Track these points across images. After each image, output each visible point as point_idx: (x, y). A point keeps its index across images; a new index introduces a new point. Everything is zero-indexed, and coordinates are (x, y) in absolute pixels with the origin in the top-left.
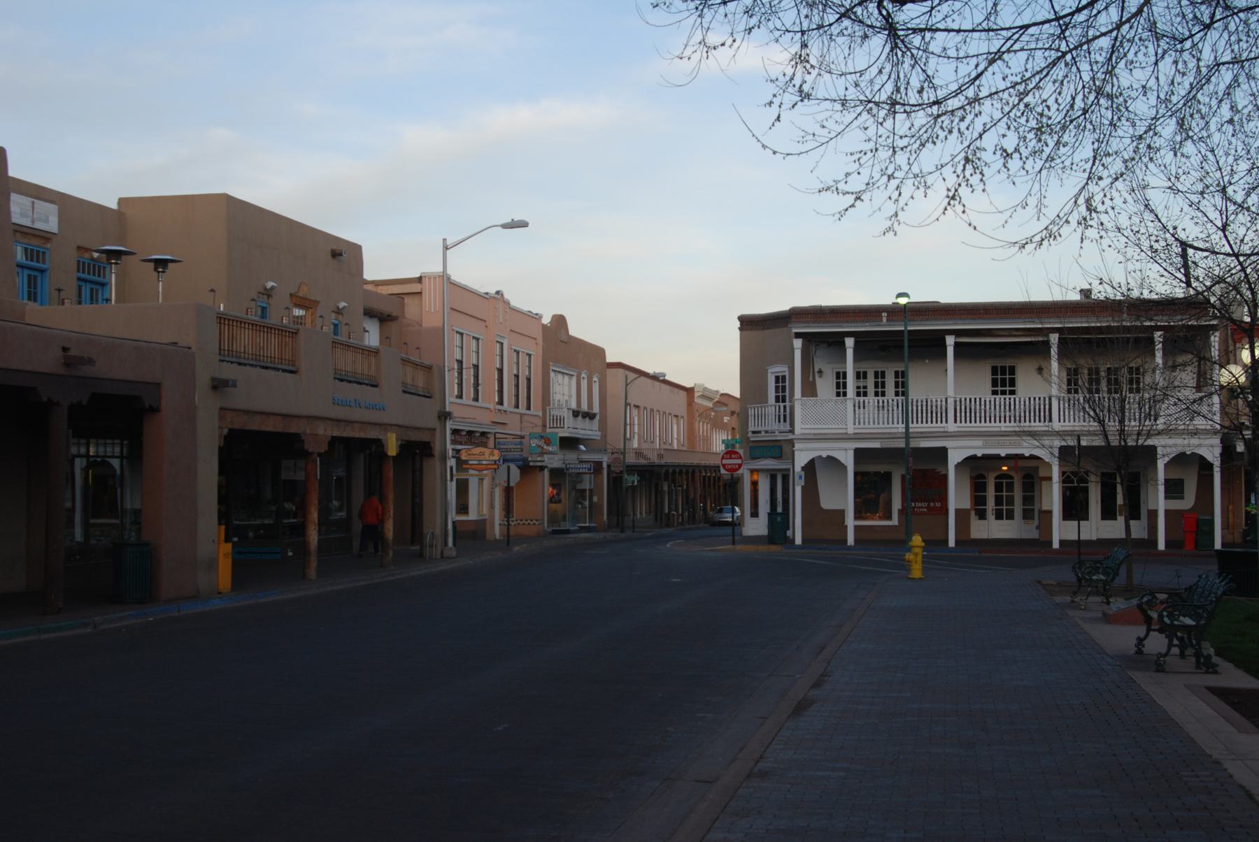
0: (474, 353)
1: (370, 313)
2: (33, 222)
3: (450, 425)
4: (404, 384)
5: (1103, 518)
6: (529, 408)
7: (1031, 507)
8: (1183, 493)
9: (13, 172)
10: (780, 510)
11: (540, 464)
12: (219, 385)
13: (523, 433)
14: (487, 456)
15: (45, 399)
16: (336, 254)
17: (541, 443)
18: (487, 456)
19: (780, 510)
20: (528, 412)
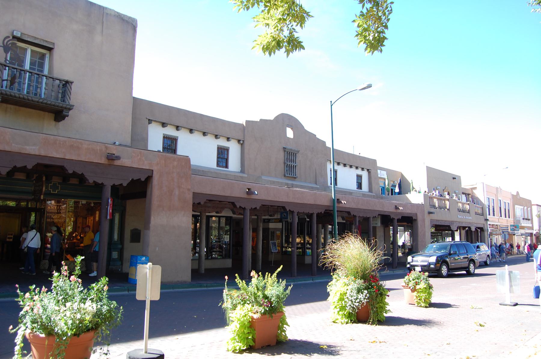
0: (38, 100)
1: (463, 193)
2: (381, 176)
3: (489, 223)
4: (476, 212)
5: (192, 215)
6: (509, 218)
7: (31, 66)
8: (135, 290)
9: (378, 165)
10: (116, 237)
11: (514, 234)
12: (430, 213)
13: (508, 225)
14: (498, 231)
15: (392, 218)
16: (454, 178)
17: (514, 227)
18: (498, 231)
19: (116, 237)
20: (509, 219)
